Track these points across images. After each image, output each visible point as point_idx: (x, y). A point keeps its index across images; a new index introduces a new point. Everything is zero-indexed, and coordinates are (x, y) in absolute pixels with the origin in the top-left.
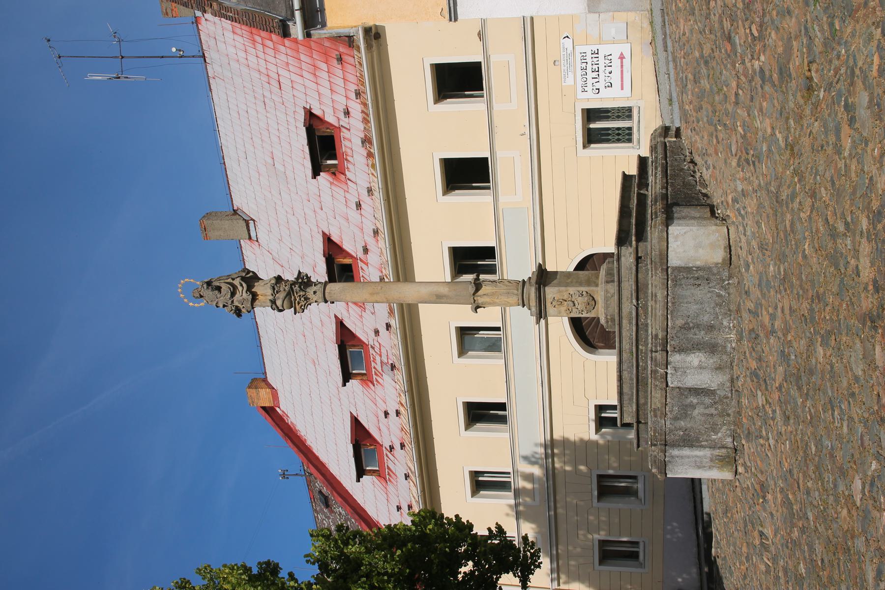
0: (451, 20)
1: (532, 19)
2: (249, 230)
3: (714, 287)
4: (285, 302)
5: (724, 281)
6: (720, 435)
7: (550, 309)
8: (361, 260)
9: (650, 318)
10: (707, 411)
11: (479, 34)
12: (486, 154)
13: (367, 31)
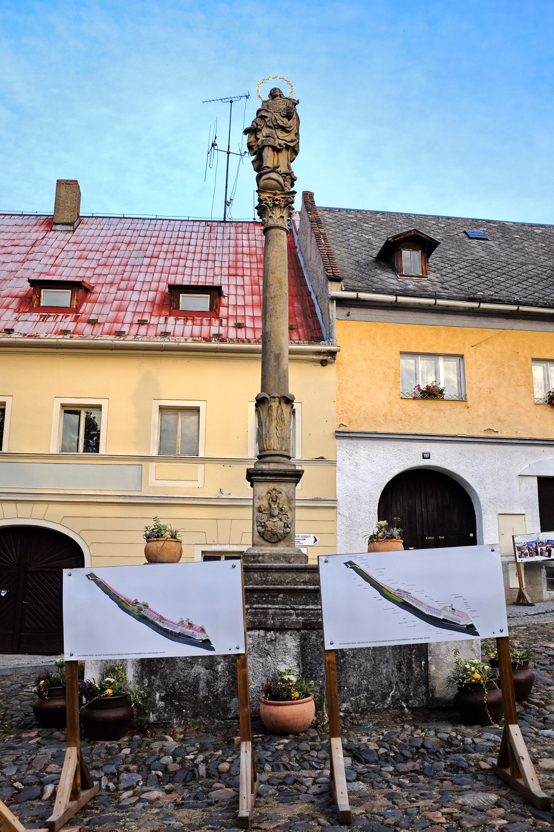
0: (337, 432)
1: (335, 508)
2: (63, 224)
3: (398, 689)
4: (274, 183)
5: (406, 701)
6: (161, 704)
7: (263, 489)
9: (281, 606)
10: (202, 684)
11: (322, 458)
12: (102, 450)
13: (333, 354)
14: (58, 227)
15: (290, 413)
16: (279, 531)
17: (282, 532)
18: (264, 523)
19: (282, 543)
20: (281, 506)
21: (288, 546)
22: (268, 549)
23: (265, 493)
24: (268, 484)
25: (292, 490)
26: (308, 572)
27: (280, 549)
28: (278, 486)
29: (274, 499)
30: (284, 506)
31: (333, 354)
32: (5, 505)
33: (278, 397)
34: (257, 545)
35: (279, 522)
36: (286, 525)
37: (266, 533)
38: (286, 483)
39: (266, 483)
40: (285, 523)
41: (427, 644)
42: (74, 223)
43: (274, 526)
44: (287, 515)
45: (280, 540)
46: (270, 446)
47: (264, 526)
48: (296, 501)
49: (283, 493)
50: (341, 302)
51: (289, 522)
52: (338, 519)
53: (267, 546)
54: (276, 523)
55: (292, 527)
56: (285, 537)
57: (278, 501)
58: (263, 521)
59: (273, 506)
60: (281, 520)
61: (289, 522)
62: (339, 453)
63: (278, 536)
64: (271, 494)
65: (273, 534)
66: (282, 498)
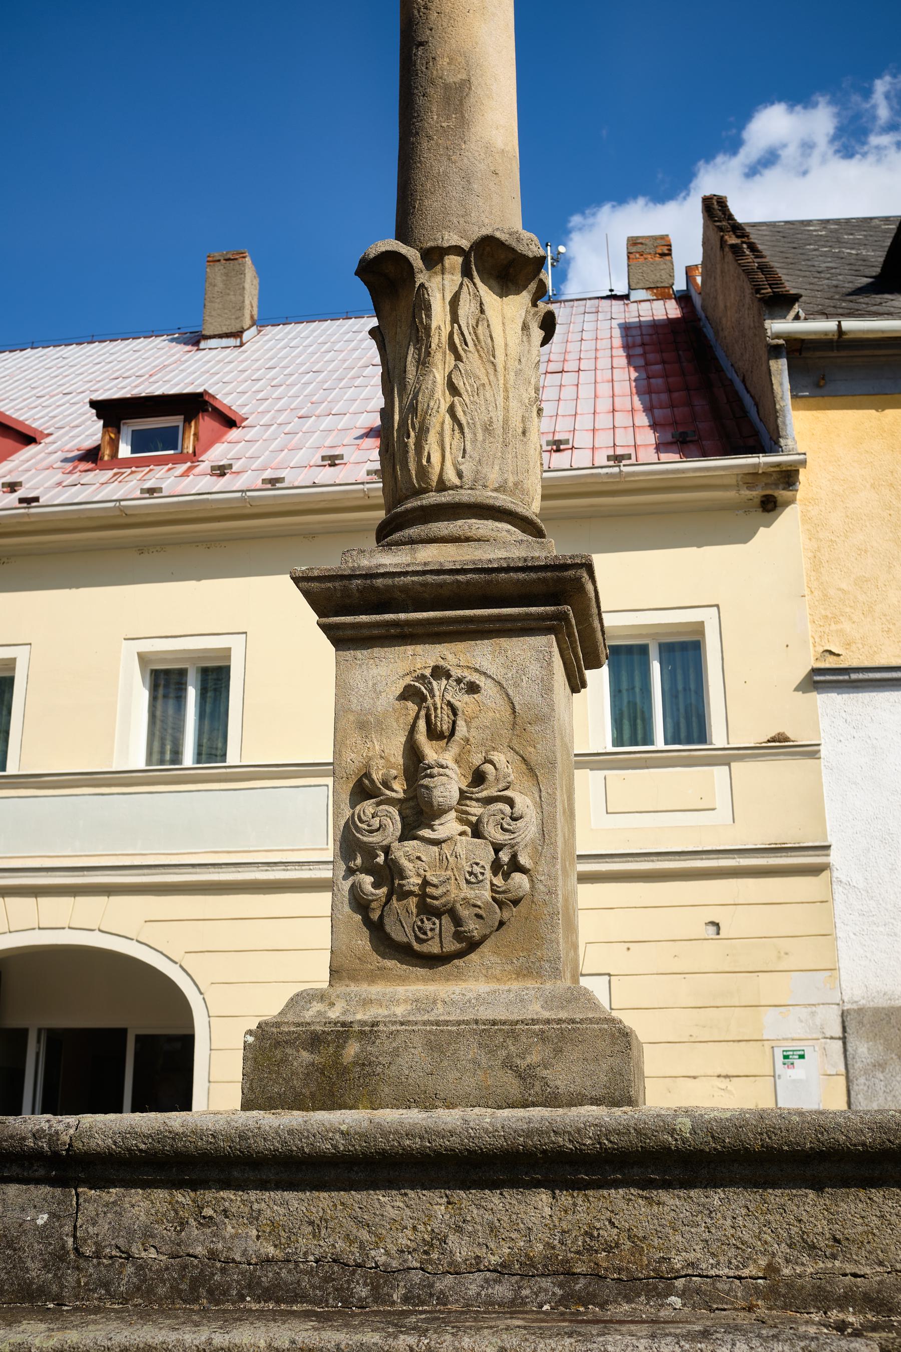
2: (220, 336)
8: (190, 469)
11: (781, 738)
14: (213, 343)
15: (525, 327)
16: (467, 892)
18: (387, 850)
20: (477, 759)
21: (524, 973)
22: (401, 997)
26: (552, 1184)
27: (474, 992)
28: (453, 655)
30: (496, 757)
31: (788, 477)
32: (13, 902)
33: (456, 250)
34: (354, 977)
35: (467, 839)
36: (505, 857)
40: (497, 848)
42: (242, 332)
44: (510, 802)
45: (473, 945)
46: (423, 472)
47: (389, 874)
50: (797, 349)
52: (836, 896)
53: (403, 979)
55: (543, 867)
56: (502, 924)
60: (477, 833)
62: (824, 724)
63: (457, 921)
66: (481, 714)
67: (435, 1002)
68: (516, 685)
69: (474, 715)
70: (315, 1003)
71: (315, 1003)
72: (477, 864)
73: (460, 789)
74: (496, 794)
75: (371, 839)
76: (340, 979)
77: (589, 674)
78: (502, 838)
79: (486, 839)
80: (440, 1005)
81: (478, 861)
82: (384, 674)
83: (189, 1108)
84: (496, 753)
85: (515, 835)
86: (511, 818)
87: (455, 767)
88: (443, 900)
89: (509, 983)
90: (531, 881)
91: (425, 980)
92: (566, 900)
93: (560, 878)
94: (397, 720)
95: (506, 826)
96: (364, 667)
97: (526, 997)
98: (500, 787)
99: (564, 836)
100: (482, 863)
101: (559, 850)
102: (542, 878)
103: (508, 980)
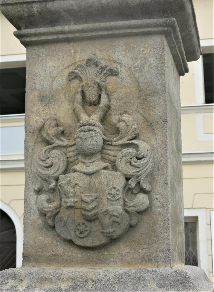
17: (117, 208)
19: (122, 249)
21: (147, 260)
23: (62, 80)
24: (71, 48)
25: (152, 61)
28: (101, 52)
29: (92, 95)
36: (132, 183)
37: (64, 214)
38: (130, 40)
39: (65, 46)
41: (186, 264)
43: (90, 188)
44: (136, 146)
45: (113, 241)
48: (183, 156)
49: (124, 73)
51: (144, 172)
53: (69, 262)
54: (95, 180)
55: (159, 189)
57: (104, 100)
58: (51, 172)
59: (84, 118)
61: (144, 172)
63: (103, 226)
64: (81, 80)
65: (90, 220)
67: (87, 281)
68: (141, 70)
69: (113, 91)
70: (10, 280)
71: (10, 280)
72: (114, 188)
73: (103, 139)
74: (127, 142)
75: (47, 172)
76: (29, 261)
77: (190, 64)
78: (131, 171)
79: (120, 171)
80: (90, 283)
81: (115, 186)
82: (56, 65)
83: (15, 266)
84: (126, 115)
85: (140, 169)
86: (137, 157)
87: (100, 125)
88: (93, 212)
89: (137, 266)
90: (150, 199)
91: (83, 263)
92: (174, 208)
93: (170, 196)
94: (65, 95)
95: (133, 164)
96: (44, 61)
97: (146, 278)
98: (130, 137)
99: (173, 167)
100: (117, 187)
101: (169, 178)
102: (158, 197)
103: (136, 264)
